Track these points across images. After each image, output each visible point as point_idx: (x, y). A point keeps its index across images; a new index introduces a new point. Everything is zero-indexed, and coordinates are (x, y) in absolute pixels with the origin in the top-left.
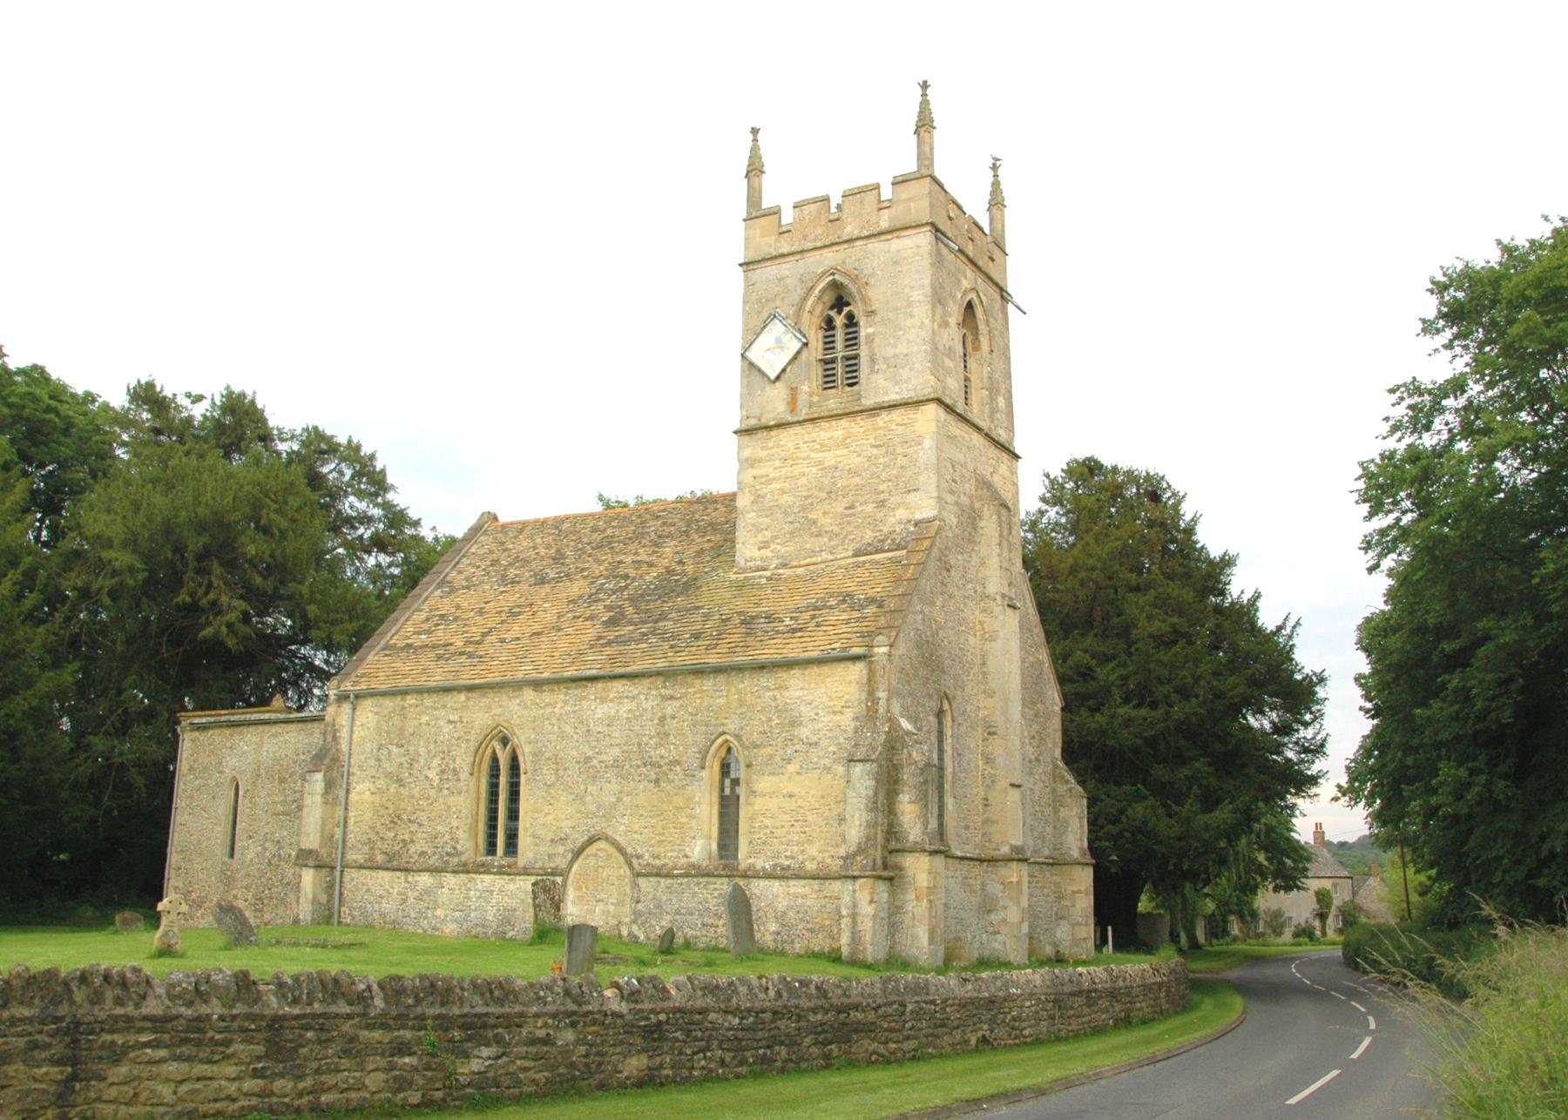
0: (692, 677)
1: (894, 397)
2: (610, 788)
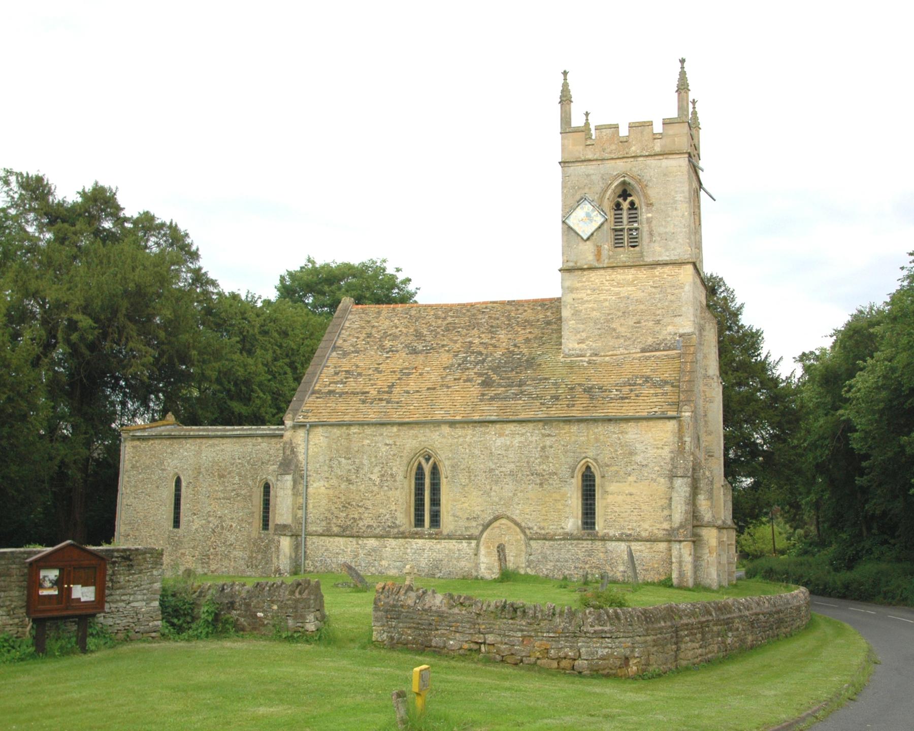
1: (665, 258)
2: (508, 488)
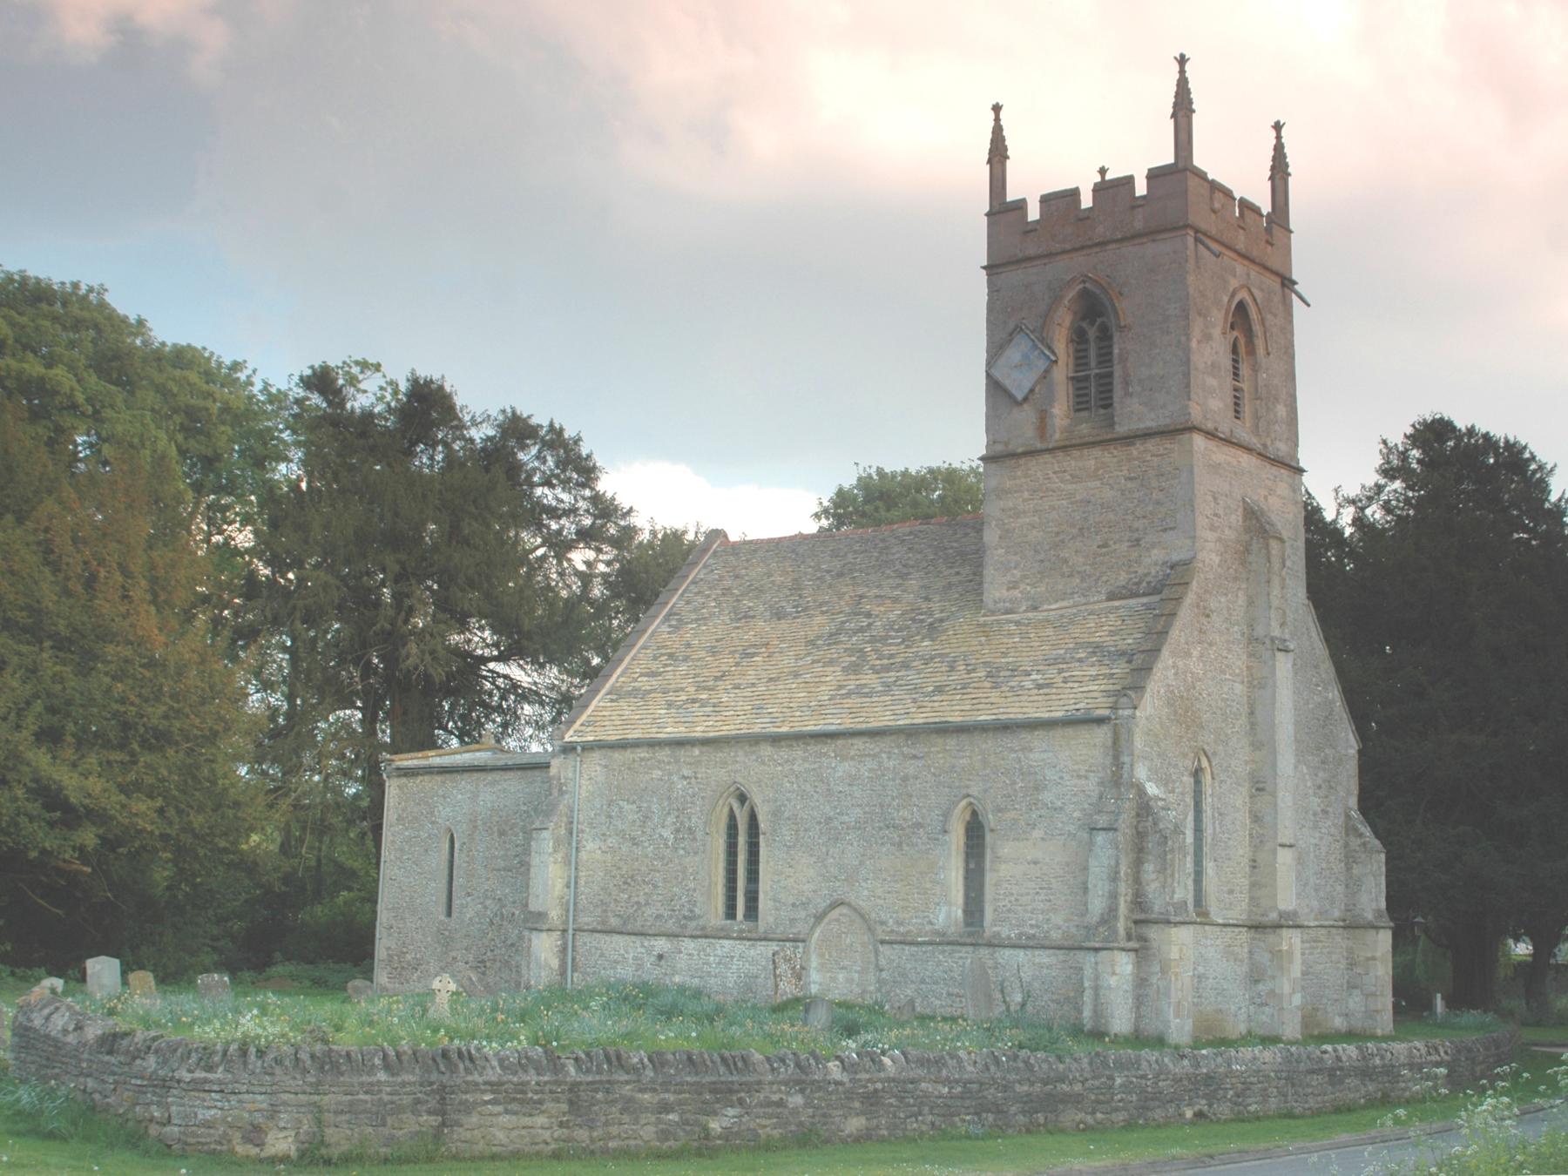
0: (934, 736)
1: (1150, 423)
